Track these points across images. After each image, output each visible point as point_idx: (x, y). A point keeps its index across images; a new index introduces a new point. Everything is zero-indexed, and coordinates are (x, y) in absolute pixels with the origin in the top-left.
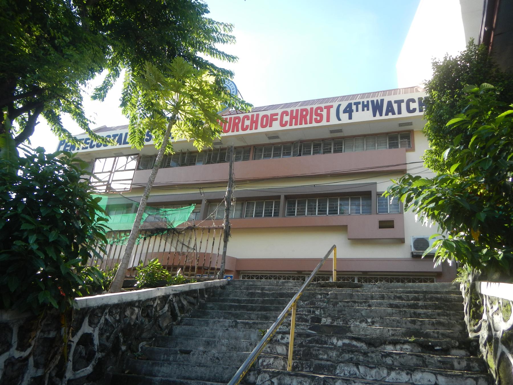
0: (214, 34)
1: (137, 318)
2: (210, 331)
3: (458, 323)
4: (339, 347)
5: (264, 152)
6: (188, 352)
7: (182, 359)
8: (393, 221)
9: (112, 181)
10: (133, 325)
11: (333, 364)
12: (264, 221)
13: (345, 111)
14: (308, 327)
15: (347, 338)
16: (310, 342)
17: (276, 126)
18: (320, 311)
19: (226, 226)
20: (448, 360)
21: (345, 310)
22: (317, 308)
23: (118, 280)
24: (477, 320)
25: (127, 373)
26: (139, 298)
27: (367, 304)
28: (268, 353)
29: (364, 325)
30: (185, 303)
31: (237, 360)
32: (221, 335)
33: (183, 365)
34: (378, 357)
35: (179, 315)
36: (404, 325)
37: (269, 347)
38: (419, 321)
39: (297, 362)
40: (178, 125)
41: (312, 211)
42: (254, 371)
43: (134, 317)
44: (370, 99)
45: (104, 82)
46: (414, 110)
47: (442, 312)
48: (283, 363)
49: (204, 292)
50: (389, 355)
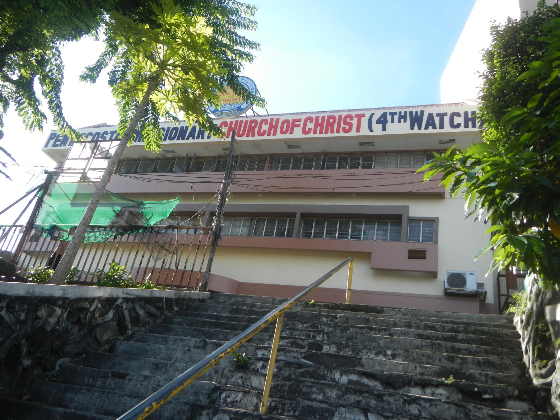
0: (234, 17)
1: (58, 323)
2: (165, 351)
3: (515, 364)
4: (343, 384)
5: (282, 163)
6: (123, 376)
7: (113, 386)
8: (425, 251)
9: (90, 169)
10: (51, 331)
11: (330, 407)
12: (275, 241)
13: (378, 122)
14: (303, 355)
15: (354, 373)
16: (302, 375)
17: (298, 133)
18: (323, 336)
19: (217, 226)
20: (505, 416)
21: (356, 338)
22: (319, 332)
23: (57, 277)
24: (545, 361)
25: (26, 400)
26: (64, 294)
27: (388, 333)
28: (238, 385)
29: (381, 358)
30: (141, 312)
31: (190, 392)
32: (179, 358)
33: (108, 393)
34: (398, 402)
35: (130, 327)
36: (437, 362)
37: (241, 378)
38: (458, 357)
39: (275, 401)
40: (164, 93)
41: (331, 234)
42: (209, 409)
43: (53, 320)
44: (408, 110)
45: (99, 61)
46: (459, 125)
47: (491, 349)
48: (255, 400)
49: (174, 303)
50: (415, 400)
